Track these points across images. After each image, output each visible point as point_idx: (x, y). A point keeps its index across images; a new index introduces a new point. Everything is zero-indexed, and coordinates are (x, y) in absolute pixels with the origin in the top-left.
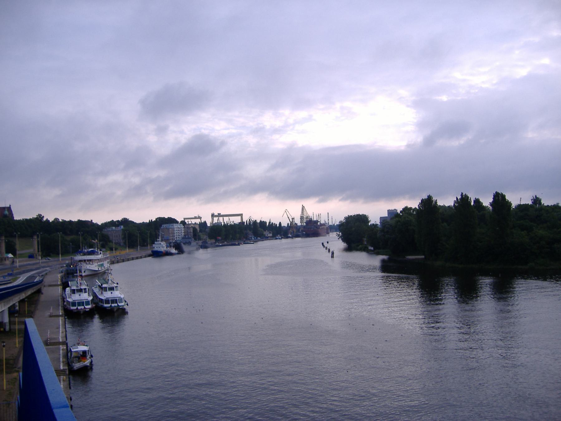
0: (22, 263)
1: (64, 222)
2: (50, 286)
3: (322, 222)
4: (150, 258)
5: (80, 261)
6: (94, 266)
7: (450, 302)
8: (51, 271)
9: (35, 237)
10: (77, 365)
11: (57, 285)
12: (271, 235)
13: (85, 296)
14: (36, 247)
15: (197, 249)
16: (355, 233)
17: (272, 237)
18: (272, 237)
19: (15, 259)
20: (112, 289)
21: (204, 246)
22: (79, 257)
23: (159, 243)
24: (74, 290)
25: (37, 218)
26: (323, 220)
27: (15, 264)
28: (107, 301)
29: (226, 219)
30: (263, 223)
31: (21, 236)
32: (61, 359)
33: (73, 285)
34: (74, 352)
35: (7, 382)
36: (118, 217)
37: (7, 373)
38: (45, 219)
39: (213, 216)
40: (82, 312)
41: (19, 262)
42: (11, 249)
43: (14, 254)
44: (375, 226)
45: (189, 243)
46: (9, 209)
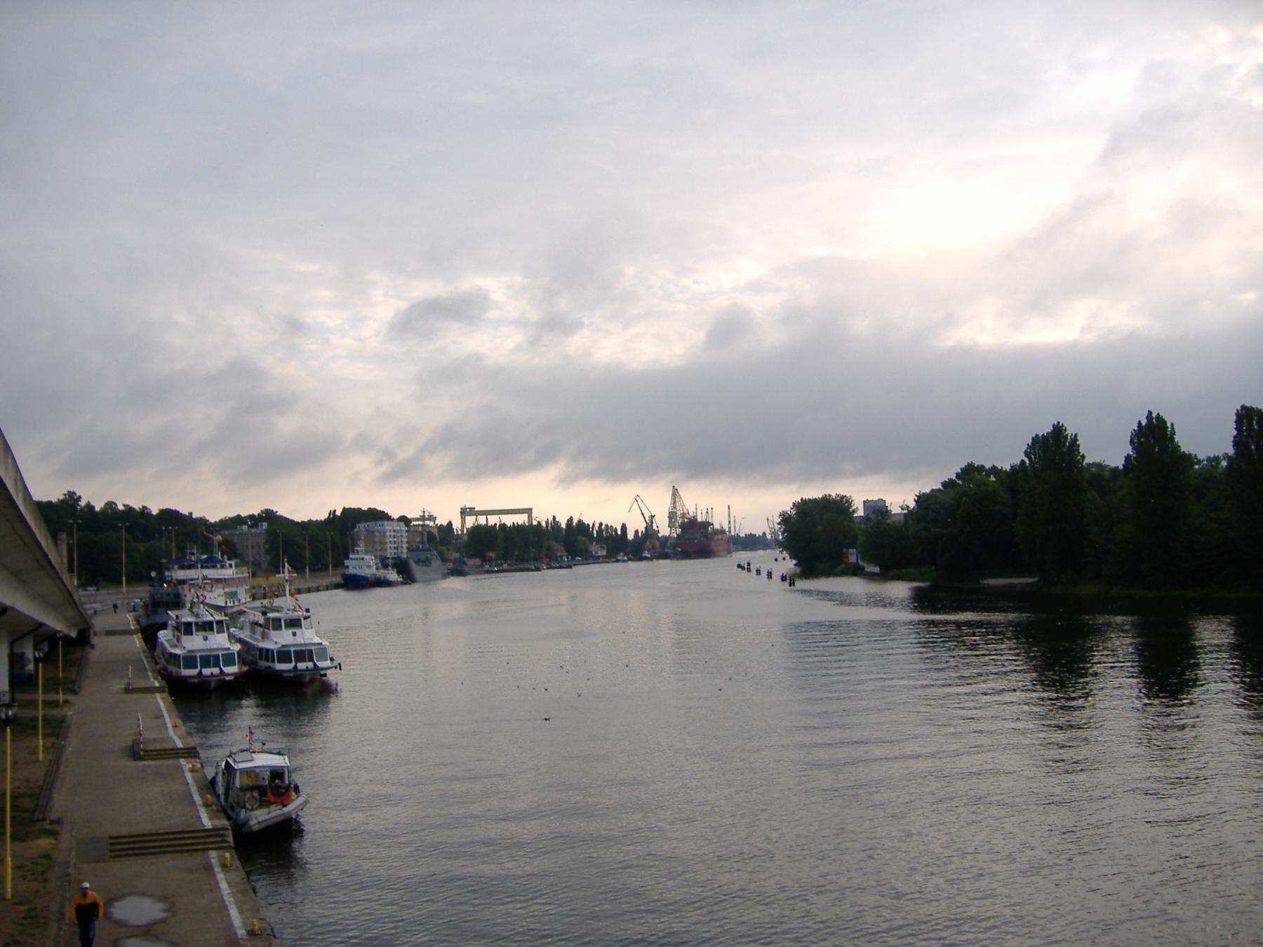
2: (110, 633)
3: (717, 526)
4: (340, 592)
7: (1115, 689)
10: (260, 817)
11: (130, 632)
12: (604, 553)
13: (219, 641)
15: (445, 576)
16: (820, 540)
17: (606, 557)
18: (606, 557)
20: (294, 623)
21: (458, 572)
23: (360, 556)
24: (189, 625)
25: (62, 502)
26: (719, 521)
28: (284, 655)
29: (493, 520)
30: (582, 528)
32: (197, 797)
34: (242, 771)
35: (17, 868)
36: (252, 508)
37: (14, 838)
38: (83, 503)
39: (465, 512)
40: (213, 685)
45: (427, 562)
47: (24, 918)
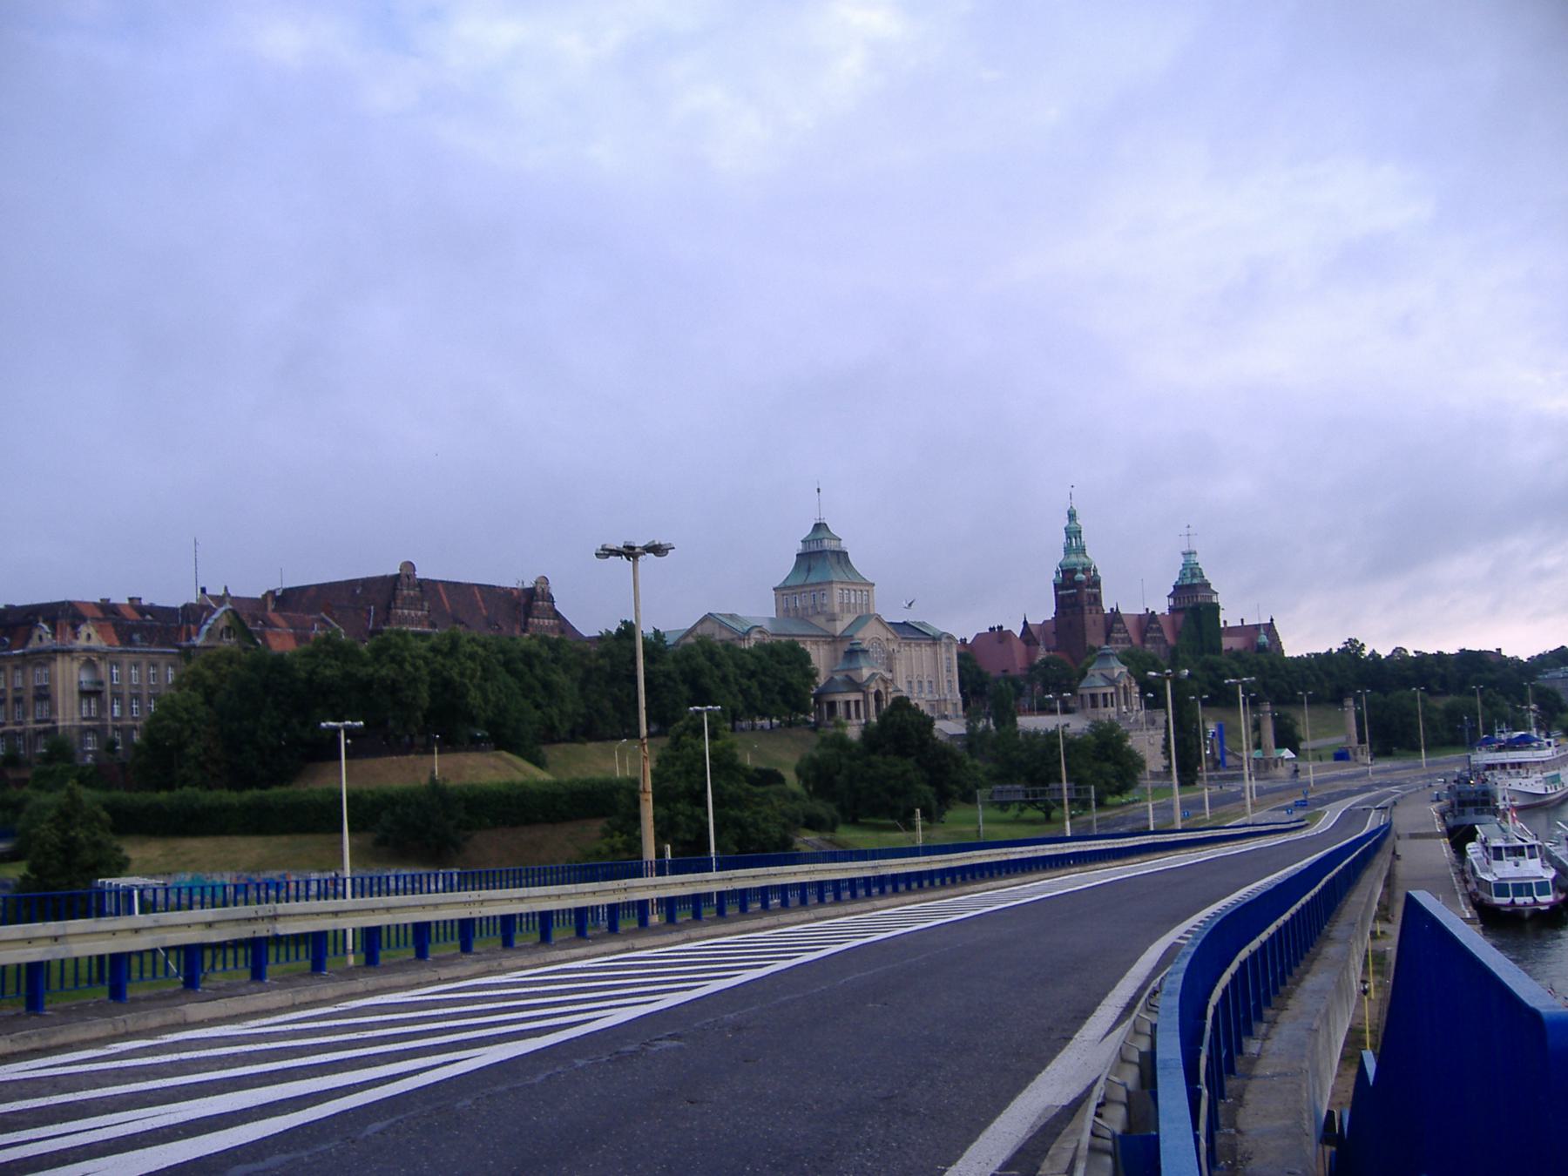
0: (1320, 775)
1: (1422, 657)
2: (1413, 836)
5: (1491, 767)
6: (1531, 781)
8: (1411, 794)
9: (1350, 702)
13: (1533, 868)
14: (1354, 730)
19: (1301, 765)
22: (1483, 757)
24: (1498, 849)
27: (1302, 778)
31: (1314, 701)
33: (1488, 831)
38: (1367, 652)
40: (1527, 914)
41: (1315, 770)
42: (1287, 738)
43: (1295, 750)
44: (1148, 621)
46: (1270, 627)
47: (507, 665)
